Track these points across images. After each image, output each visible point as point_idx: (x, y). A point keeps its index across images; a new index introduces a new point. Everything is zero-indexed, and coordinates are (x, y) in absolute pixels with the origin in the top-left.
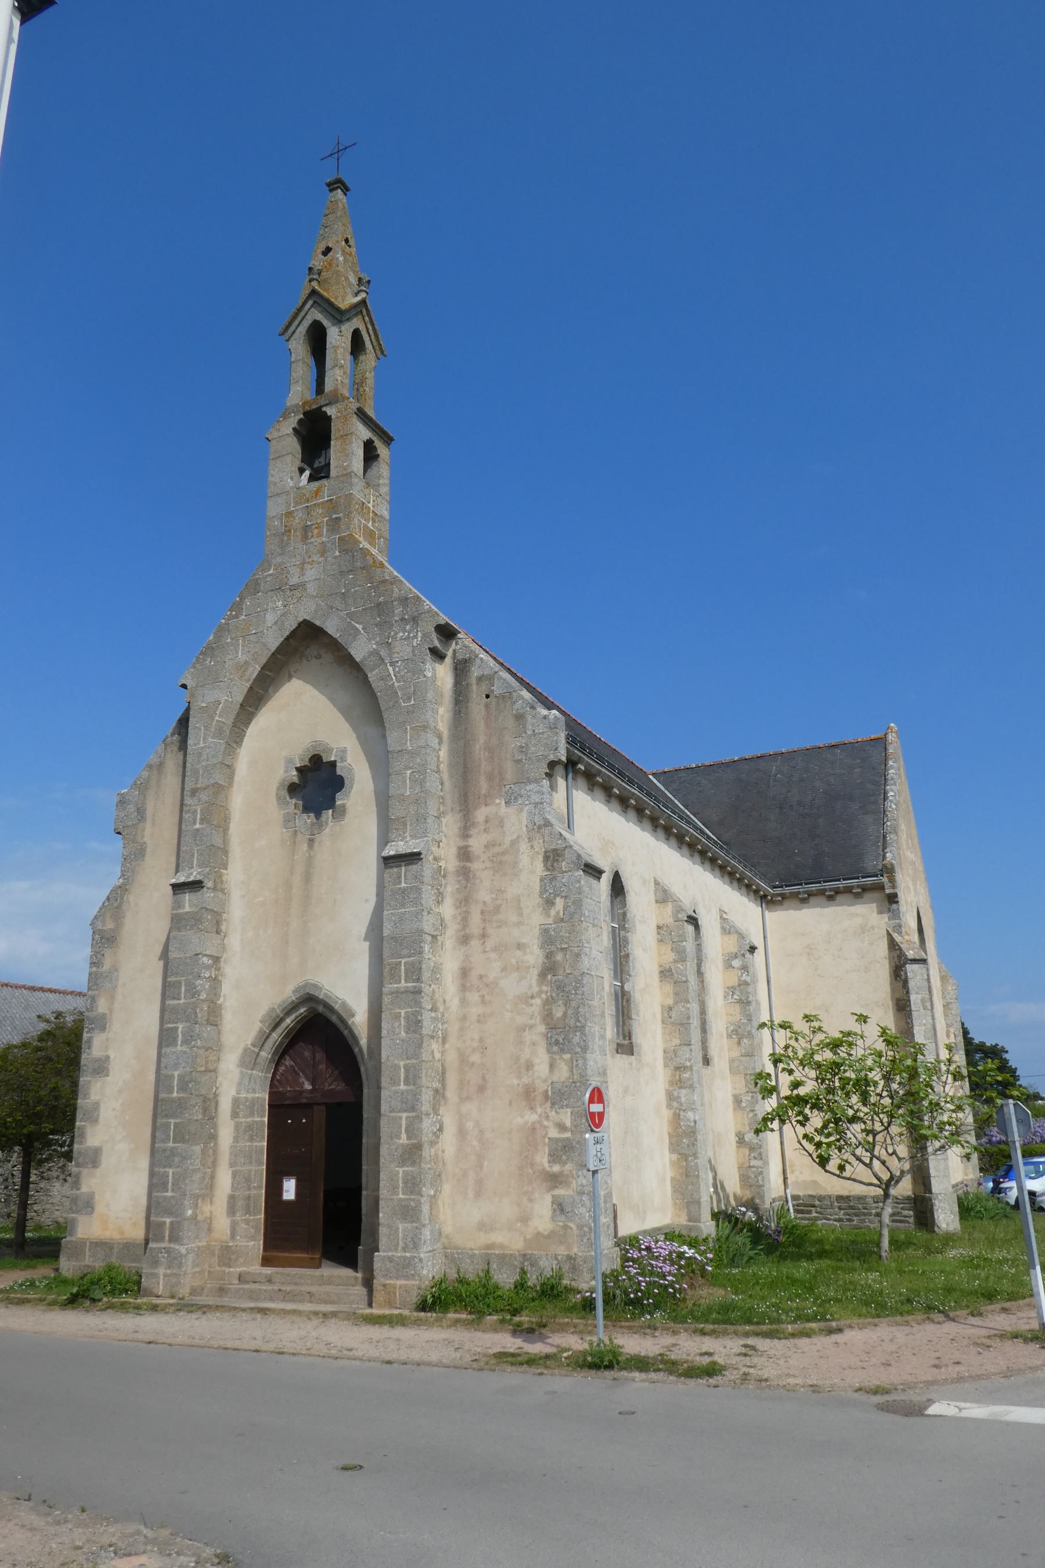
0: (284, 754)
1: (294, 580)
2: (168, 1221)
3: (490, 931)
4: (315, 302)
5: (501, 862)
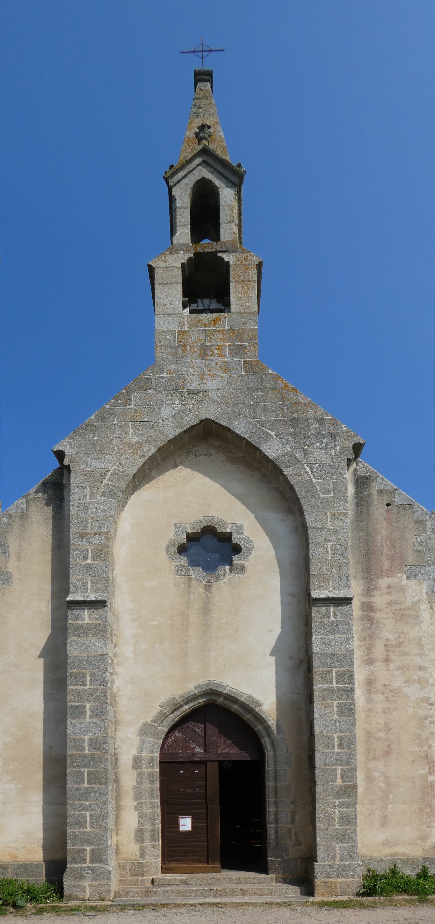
0: (173, 522)
1: (194, 384)
2: (88, 848)
3: (392, 657)
4: (204, 161)
5: (403, 615)
